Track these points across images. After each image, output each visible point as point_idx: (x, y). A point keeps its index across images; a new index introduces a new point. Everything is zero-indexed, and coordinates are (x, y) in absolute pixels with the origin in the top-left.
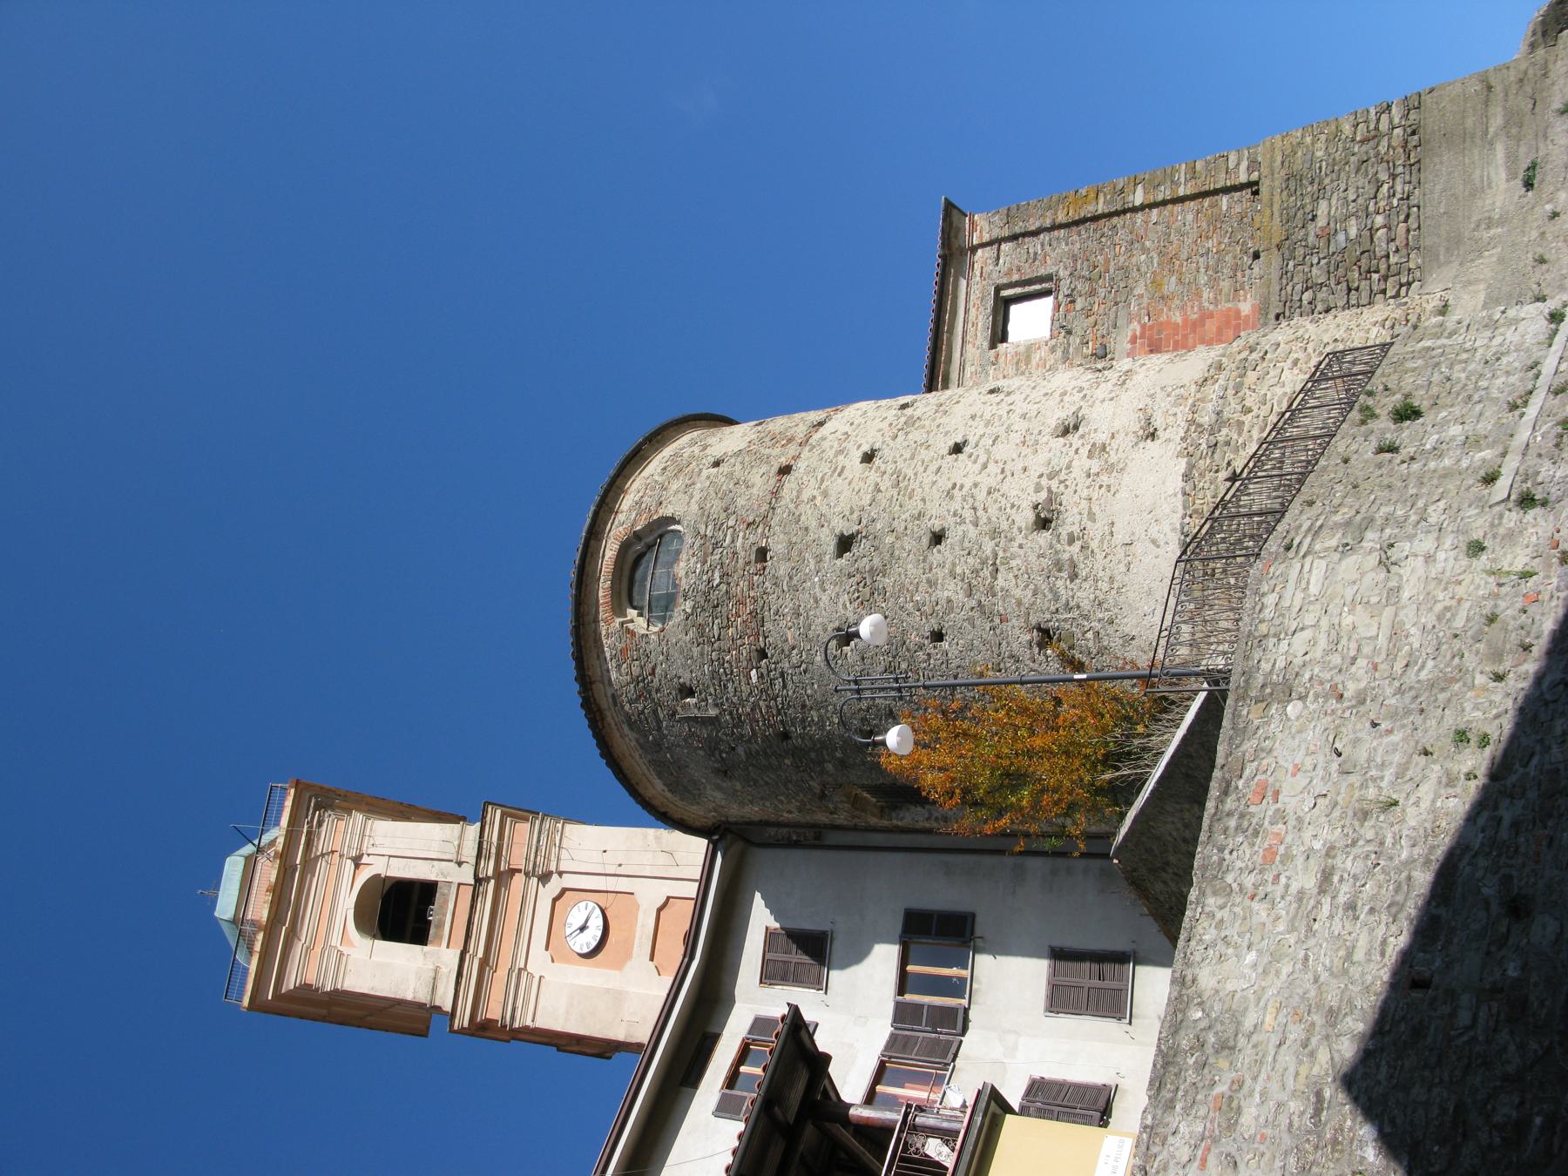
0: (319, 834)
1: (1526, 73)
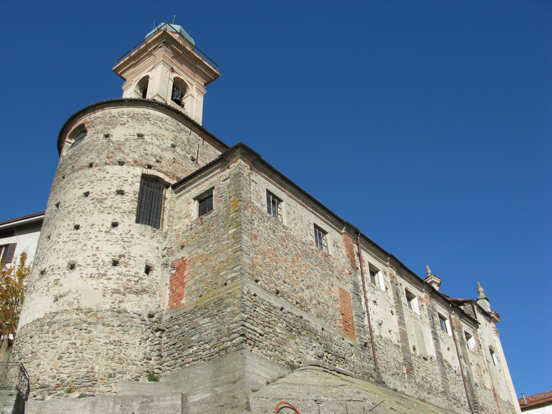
0: (158, 50)
1: (237, 398)
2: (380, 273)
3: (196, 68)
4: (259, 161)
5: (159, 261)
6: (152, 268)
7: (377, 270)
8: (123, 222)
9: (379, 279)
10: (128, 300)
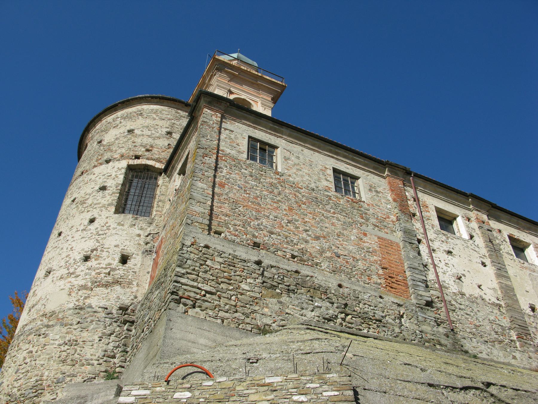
2: (459, 220)
3: (258, 85)
4: (234, 108)
5: (140, 249)
6: (129, 258)
7: (454, 216)
8: (101, 216)
9: (459, 226)
10: (95, 294)
